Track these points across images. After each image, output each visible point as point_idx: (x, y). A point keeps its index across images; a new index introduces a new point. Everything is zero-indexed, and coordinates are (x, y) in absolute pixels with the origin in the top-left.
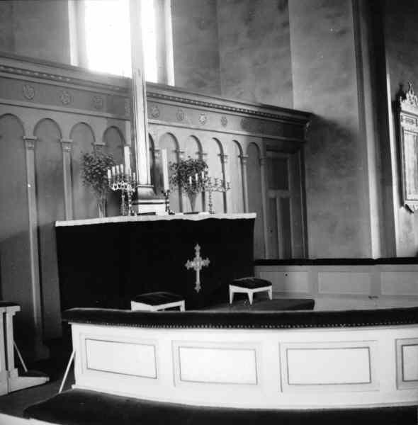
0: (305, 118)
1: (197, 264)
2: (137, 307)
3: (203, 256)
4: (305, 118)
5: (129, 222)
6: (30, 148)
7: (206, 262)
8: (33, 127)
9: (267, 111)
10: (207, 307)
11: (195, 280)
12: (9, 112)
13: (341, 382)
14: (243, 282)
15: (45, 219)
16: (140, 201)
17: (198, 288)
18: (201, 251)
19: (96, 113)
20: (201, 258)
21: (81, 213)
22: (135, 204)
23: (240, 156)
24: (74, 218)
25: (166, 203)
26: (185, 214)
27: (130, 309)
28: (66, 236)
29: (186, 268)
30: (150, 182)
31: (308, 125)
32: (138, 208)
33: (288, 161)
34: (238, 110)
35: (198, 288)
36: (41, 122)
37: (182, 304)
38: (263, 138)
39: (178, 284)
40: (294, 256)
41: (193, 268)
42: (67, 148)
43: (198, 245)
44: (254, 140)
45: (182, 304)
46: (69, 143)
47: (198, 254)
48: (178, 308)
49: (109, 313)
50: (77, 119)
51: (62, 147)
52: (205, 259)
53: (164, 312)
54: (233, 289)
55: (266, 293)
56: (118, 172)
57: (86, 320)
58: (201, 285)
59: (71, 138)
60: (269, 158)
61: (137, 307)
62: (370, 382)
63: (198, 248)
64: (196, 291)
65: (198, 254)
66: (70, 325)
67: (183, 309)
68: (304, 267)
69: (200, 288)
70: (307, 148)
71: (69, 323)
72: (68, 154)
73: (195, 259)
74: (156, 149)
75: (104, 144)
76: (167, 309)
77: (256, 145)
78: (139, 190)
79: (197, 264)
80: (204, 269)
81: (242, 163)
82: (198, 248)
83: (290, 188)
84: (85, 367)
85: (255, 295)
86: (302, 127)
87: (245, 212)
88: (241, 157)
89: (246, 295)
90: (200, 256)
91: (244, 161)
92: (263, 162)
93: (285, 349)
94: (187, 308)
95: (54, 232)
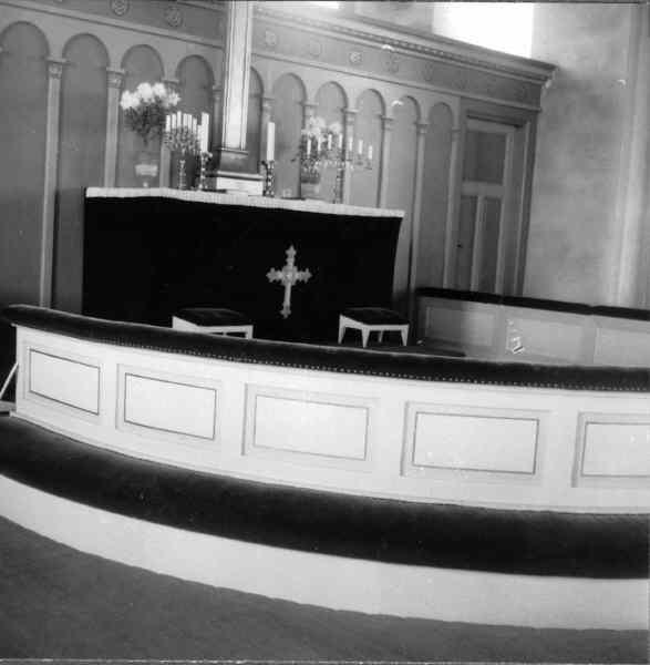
0: (540, 72)
1: (289, 275)
2: (180, 325)
3: (300, 265)
4: (540, 72)
5: (279, 209)
6: (55, 76)
7: (306, 275)
8: (120, 58)
9: (421, 43)
10: (298, 337)
11: (282, 300)
12: (25, 19)
13: (327, 453)
14: (353, 312)
15: (69, 183)
16: (219, 172)
17: (286, 312)
18: (296, 257)
19: (166, 32)
20: (295, 269)
21: (142, 180)
22: (213, 176)
23: (342, 110)
24: (116, 185)
25: (267, 180)
26: (283, 198)
27: (171, 326)
28: (98, 211)
29: (267, 279)
30: (243, 146)
31: (548, 84)
32: (215, 182)
33: (508, 140)
34: (412, 47)
35: (286, 312)
36: (76, 38)
37: (248, 330)
38: (462, 97)
39: (256, 304)
40: (498, 290)
41: (280, 281)
42: (115, 81)
43: (292, 248)
44: (446, 99)
45: (248, 330)
46: (119, 74)
47: (291, 261)
48: (242, 334)
49: (149, 332)
50: (367, 84)
51: (47, 70)
52: (304, 270)
53: (225, 336)
54: (346, 322)
55: (398, 333)
56: (179, 124)
57: (207, 352)
58: (291, 308)
59: (357, 108)
60: (468, 131)
61: (180, 325)
62: (213, 439)
63: (291, 252)
64: (283, 316)
65: (291, 261)
66: (15, 328)
67: (249, 336)
68: (489, 306)
69: (289, 312)
70: (542, 124)
71: (13, 325)
72: (58, 81)
73: (285, 268)
74: (265, 96)
75: (177, 81)
76: (229, 334)
77: (416, 102)
78: (223, 155)
79: (289, 275)
80: (298, 286)
81: (418, 133)
82: (291, 252)
83: (505, 181)
84: (27, 390)
85: (373, 335)
86: (540, 86)
87: (378, 206)
88: (418, 125)
89: (359, 332)
90: (295, 264)
91: (422, 131)
92: (456, 136)
93: (216, 387)
94: (255, 335)
95: (81, 202)
